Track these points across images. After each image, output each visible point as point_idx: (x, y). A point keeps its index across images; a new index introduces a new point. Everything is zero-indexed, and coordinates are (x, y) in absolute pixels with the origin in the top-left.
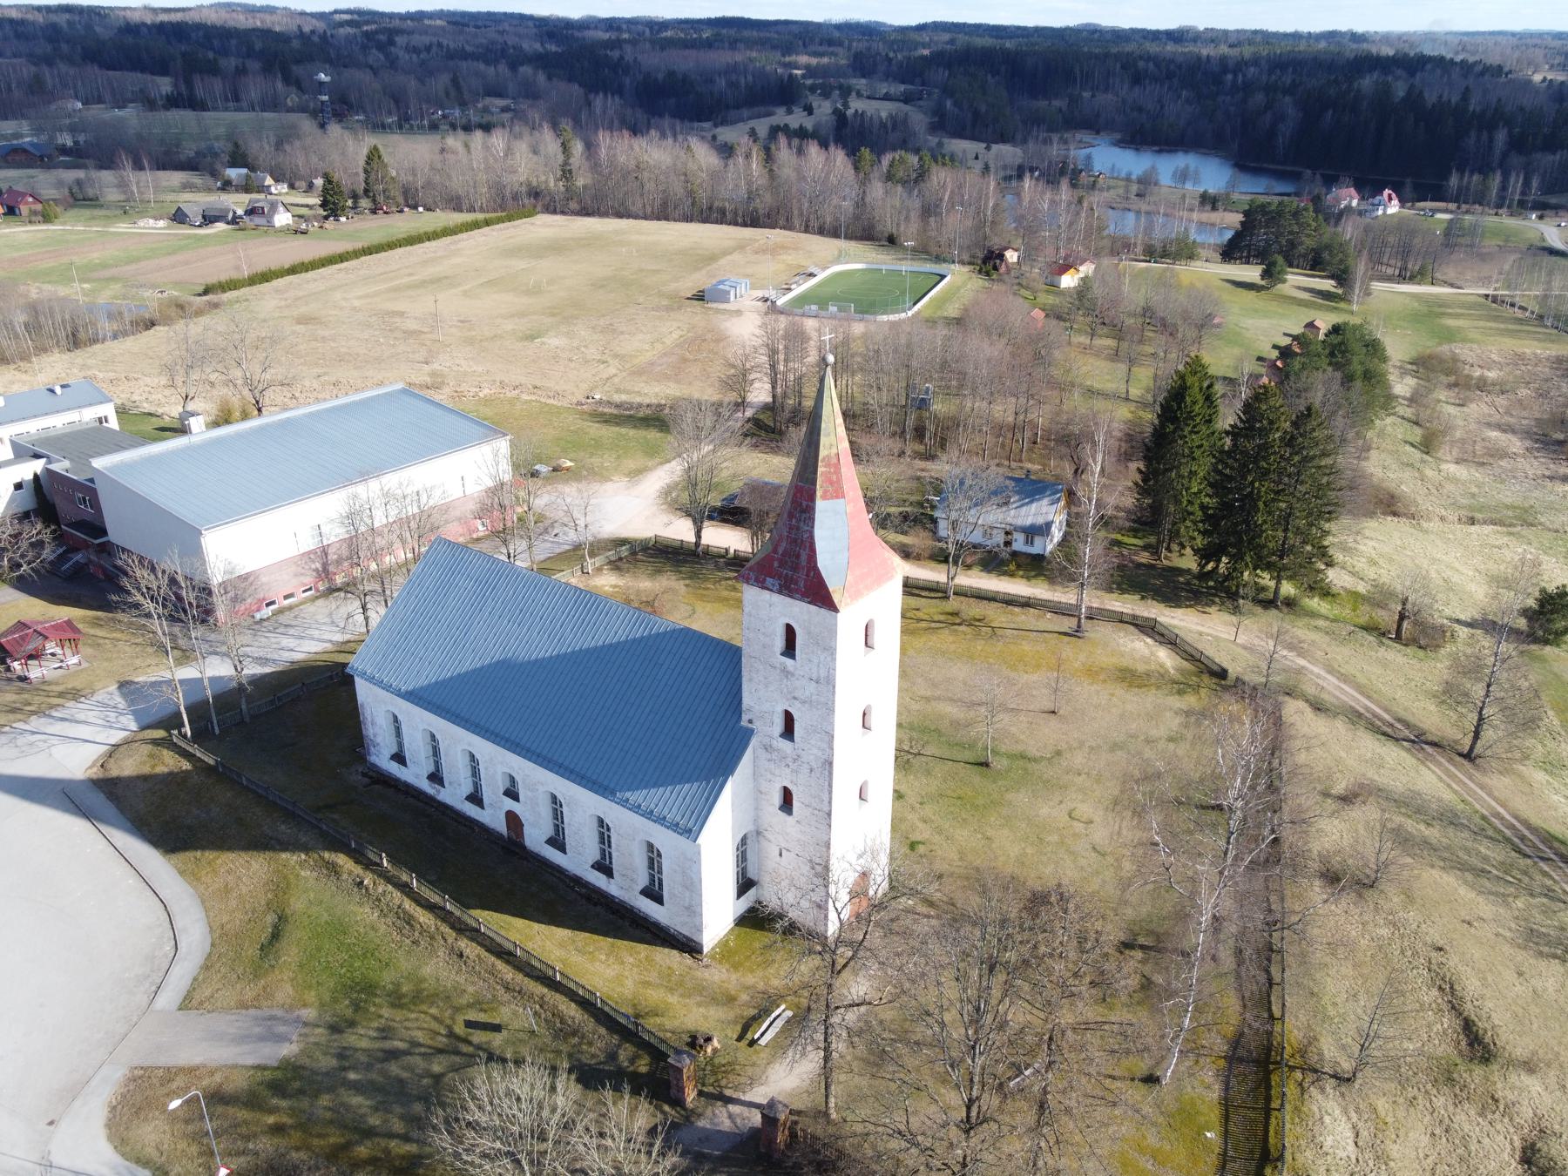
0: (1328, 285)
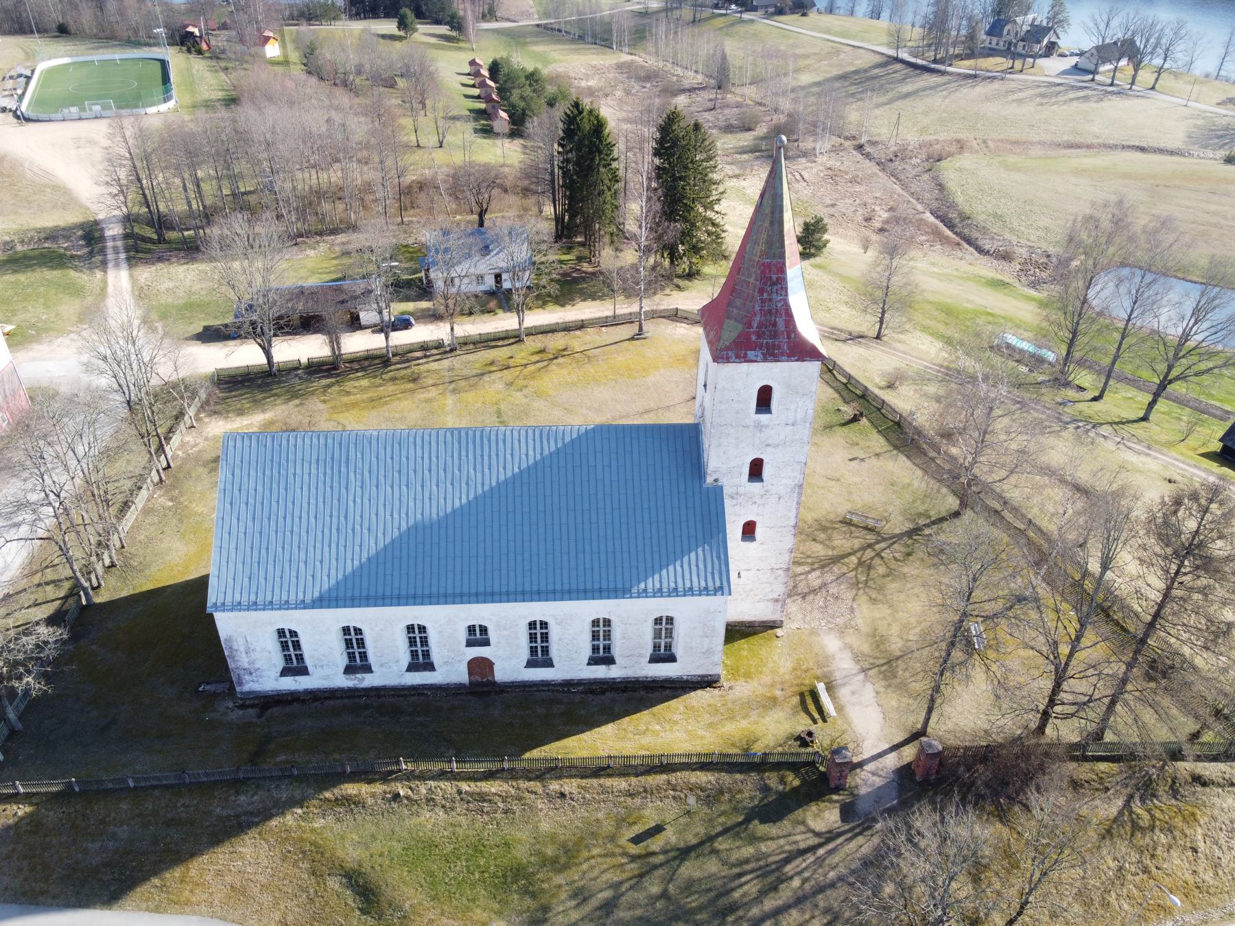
0: (443, 30)
